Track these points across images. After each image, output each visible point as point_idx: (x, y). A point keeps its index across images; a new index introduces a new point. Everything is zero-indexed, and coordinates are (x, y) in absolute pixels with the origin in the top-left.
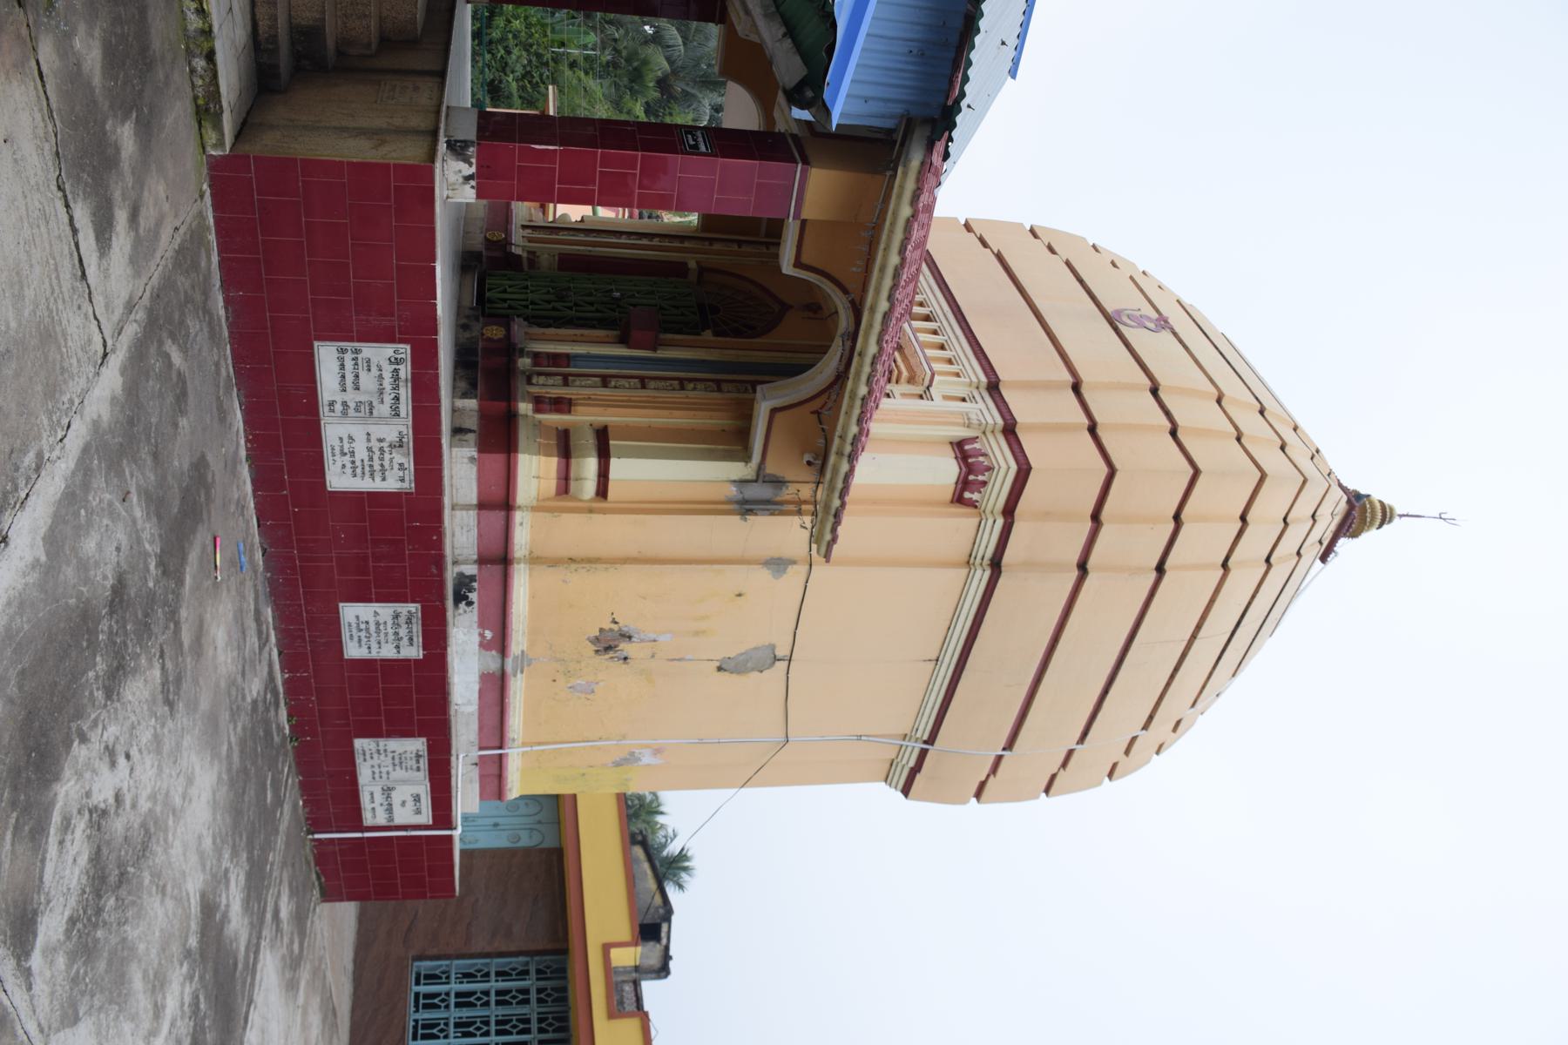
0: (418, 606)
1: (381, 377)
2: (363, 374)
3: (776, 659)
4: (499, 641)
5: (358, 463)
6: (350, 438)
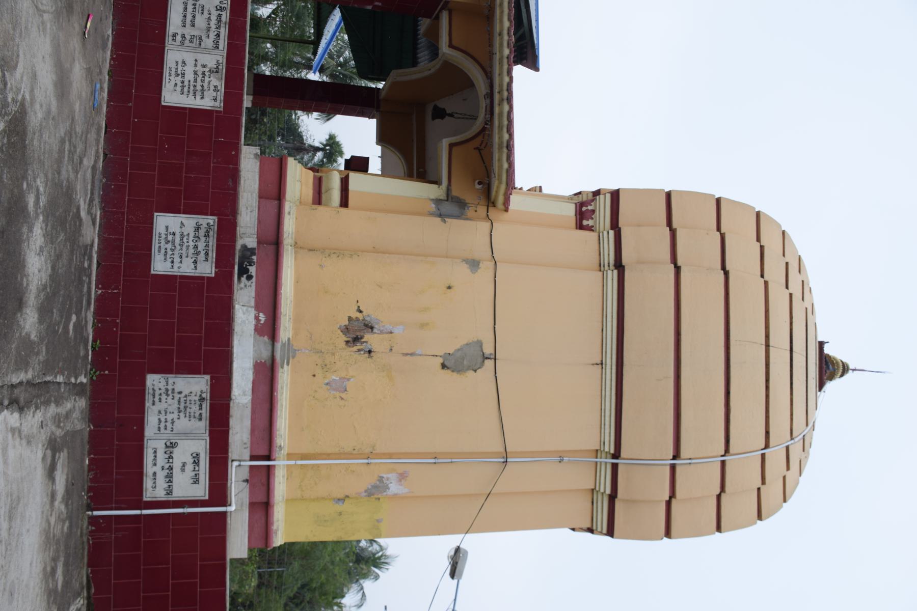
0: (215, 218)
1: (209, 19)
2: (198, 16)
4: (269, 328)
5: (186, 83)
6: (184, 62)
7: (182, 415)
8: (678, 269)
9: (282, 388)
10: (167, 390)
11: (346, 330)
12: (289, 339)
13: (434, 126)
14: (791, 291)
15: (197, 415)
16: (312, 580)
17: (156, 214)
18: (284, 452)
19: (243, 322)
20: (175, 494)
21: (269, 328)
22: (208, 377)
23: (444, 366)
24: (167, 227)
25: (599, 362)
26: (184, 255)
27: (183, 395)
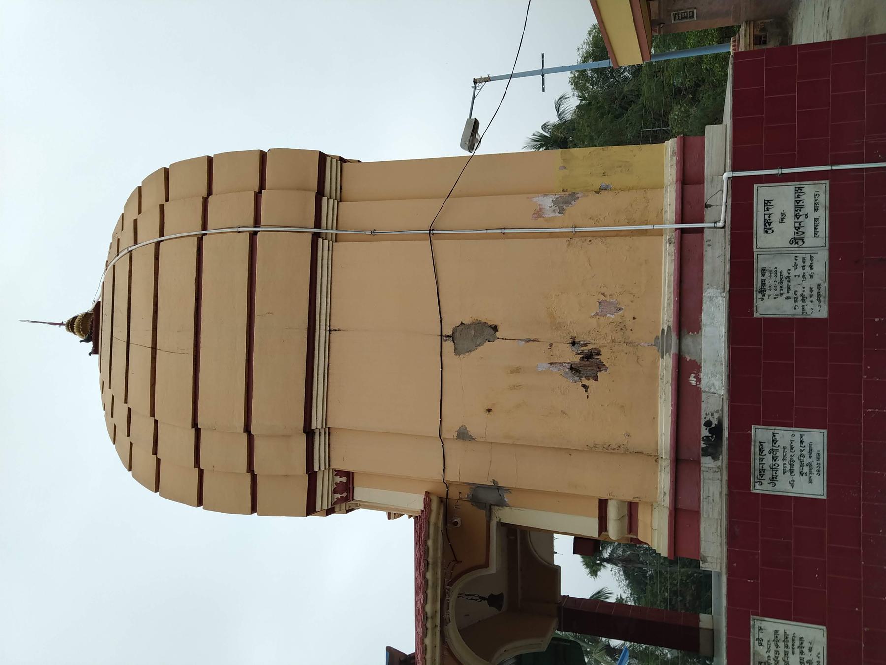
3: (452, 337)
4: (685, 369)
5: (797, 651)
7: (785, 274)
8: (247, 429)
9: (669, 305)
10: (803, 301)
11: (600, 366)
12: (662, 357)
13: (500, 587)
14: (126, 406)
15: (767, 274)
16: (612, 121)
17: (825, 497)
18: (666, 237)
19: (714, 376)
20: (793, 188)
21: (685, 369)
22: (756, 315)
23: (495, 328)
24: (810, 481)
25: (333, 332)
26: (788, 450)
27: (784, 296)
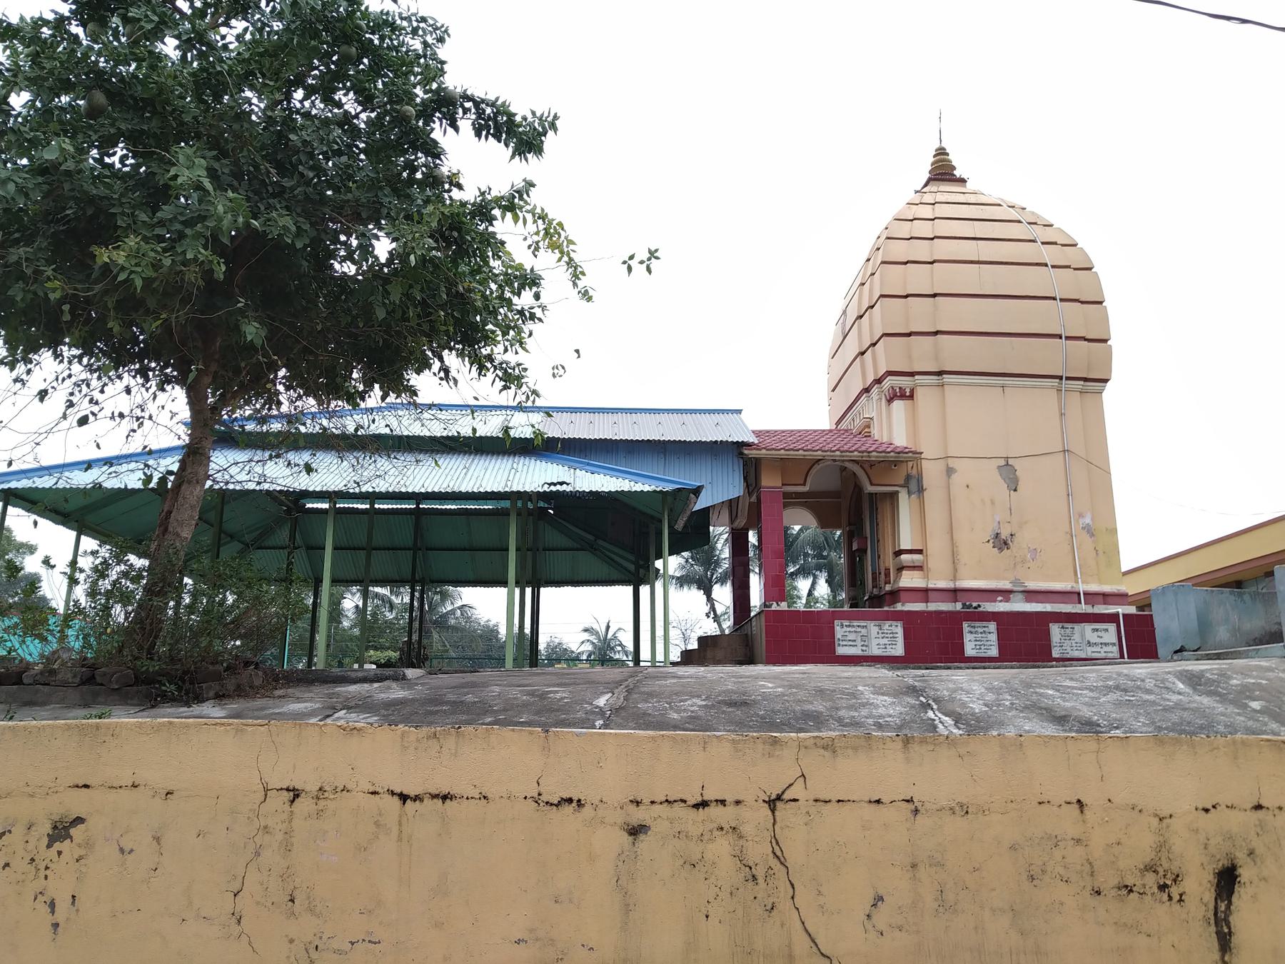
4: (1006, 594)
11: (1001, 549)
21: (1006, 594)
